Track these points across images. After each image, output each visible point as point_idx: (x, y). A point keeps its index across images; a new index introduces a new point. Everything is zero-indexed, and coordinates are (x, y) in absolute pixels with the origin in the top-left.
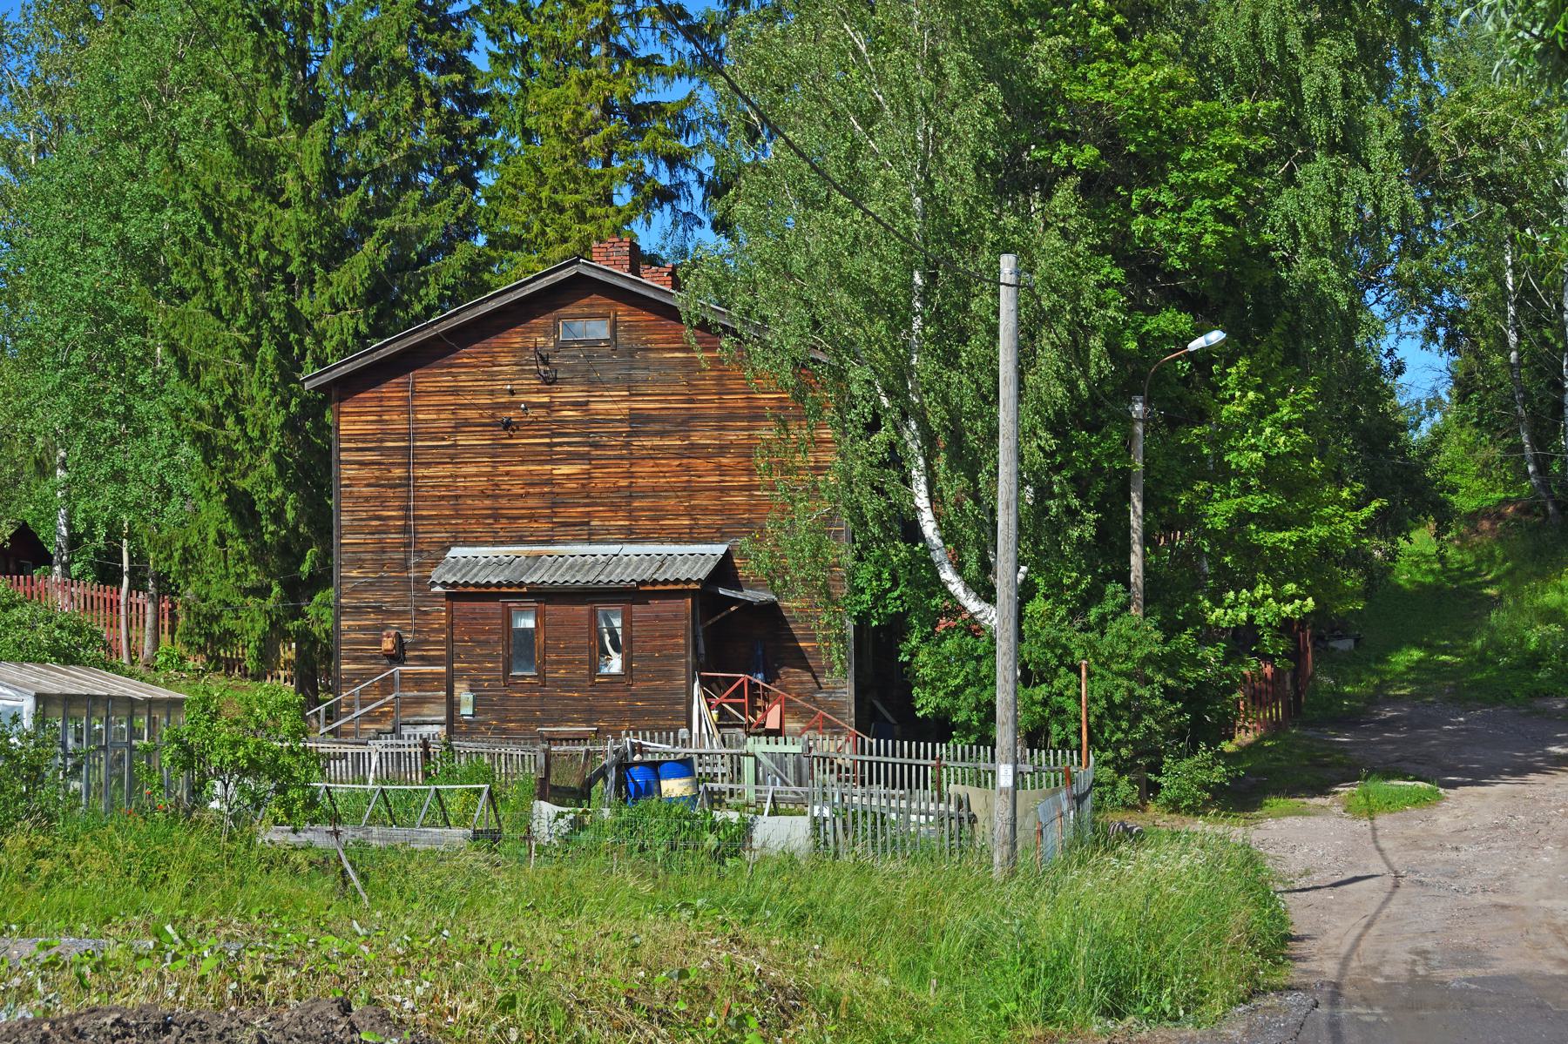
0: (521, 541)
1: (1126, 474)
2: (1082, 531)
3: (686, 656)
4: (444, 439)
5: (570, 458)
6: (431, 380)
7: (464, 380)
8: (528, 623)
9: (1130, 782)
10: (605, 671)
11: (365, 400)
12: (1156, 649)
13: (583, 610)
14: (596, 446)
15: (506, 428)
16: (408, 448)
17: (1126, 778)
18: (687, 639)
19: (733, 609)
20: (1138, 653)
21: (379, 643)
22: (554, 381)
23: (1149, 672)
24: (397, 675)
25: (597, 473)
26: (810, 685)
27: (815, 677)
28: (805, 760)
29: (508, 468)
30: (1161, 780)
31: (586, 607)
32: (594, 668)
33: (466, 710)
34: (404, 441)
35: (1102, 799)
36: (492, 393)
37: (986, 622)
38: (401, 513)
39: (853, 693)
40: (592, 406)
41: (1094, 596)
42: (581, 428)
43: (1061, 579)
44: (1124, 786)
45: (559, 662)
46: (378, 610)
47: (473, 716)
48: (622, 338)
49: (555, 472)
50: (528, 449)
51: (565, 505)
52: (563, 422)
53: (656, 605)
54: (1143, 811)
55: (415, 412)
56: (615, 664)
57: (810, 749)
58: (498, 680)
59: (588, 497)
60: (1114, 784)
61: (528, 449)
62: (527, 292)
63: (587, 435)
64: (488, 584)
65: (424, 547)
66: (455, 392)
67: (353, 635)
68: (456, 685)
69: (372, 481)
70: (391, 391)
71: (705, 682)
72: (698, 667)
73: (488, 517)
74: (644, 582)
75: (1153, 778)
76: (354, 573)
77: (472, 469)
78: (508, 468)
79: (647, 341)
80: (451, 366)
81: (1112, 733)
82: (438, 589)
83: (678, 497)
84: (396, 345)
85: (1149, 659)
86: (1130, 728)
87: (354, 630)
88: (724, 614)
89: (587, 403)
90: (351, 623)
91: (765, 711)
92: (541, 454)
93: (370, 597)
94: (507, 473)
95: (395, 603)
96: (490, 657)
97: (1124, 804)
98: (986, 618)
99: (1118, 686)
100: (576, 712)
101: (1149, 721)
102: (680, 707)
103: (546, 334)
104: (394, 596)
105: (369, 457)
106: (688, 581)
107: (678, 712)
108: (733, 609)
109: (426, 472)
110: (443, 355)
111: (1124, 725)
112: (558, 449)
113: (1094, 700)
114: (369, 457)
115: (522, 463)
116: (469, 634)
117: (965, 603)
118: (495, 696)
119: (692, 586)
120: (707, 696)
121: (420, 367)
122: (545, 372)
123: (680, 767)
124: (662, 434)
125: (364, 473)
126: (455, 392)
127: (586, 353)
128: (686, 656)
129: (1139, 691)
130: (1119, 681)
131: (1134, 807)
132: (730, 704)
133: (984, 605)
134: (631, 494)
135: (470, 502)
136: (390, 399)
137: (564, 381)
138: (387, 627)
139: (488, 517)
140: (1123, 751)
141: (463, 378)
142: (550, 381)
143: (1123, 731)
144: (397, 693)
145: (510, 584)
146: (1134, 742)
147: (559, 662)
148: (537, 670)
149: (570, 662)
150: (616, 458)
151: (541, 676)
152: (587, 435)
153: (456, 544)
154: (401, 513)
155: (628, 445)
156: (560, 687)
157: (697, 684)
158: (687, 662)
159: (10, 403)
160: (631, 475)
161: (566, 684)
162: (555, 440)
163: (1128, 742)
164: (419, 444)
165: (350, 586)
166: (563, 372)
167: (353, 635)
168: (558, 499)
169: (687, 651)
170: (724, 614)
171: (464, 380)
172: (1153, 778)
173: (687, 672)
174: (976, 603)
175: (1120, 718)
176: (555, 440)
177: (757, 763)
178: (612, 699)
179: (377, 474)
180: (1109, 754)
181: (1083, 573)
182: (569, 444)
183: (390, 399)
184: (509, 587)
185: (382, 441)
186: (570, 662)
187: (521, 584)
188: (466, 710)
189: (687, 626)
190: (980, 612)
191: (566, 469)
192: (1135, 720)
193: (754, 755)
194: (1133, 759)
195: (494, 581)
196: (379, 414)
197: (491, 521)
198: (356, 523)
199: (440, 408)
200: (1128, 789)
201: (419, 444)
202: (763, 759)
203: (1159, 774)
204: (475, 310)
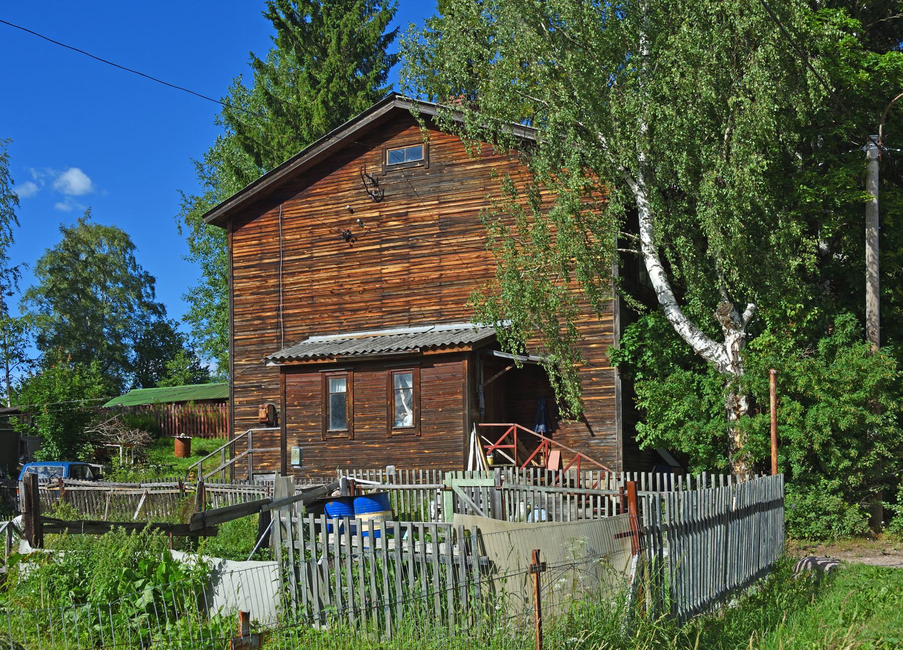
0: (358, 328)
1: (862, 207)
2: (804, 260)
3: (463, 410)
4: (304, 254)
5: (395, 259)
6: (294, 209)
7: (318, 206)
8: (343, 389)
9: (861, 510)
10: (400, 425)
11: (250, 229)
12: (889, 375)
13: (383, 375)
14: (413, 247)
15: (347, 241)
16: (278, 262)
17: (857, 505)
18: (464, 395)
19: (507, 369)
20: (870, 382)
21: (257, 414)
22: (383, 198)
23: (882, 400)
24: (250, 435)
25: (415, 269)
26: (585, 433)
27: (589, 426)
28: (498, 493)
29: (349, 272)
30: (894, 507)
31: (385, 372)
32: (391, 420)
33: (295, 461)
34: (276, 257)
35: (830, 527)
36: (337, 213)
37: (712, 359)
38: (274, 313)
39: (621, 438)
40: (411, 215)
41: (819, 330)
42: (402, 234)
43: (785, 312)
44: (853, 514)
45: (365, 420)
46: (259, 388)
47: (300, 465)
48: (433, 157)
49: (384, 271)
50: (364, 255)
51: (390, 297)
52: (390, 231)
53: (440, 368)
54: (875, 539)
55: (283, 235)
56: (408, 420)
57: (502, 481)
58: (319, 436)
59: (409, 289)
60: (841, 512)
61: (364, 255)
62: (358, 128)
63: (407, 239)
64: (306, 358)
65: (290, 337)
66: (311, 215)
67: (242, 409)
68: (288, 441)
69: (255, 290)
70: (266, 220)
71: (480, 431)
72: (473, 421)
73: (335, 311)
74: (425, 348)
75: (886, 505)
76: (243, 362)
77: (323, 275)
78: (349, 272)
79: (453, 159)
80: (309, 196)
81: (839, 461)
82: (271, 364)
83: (477, 283)
84: (265, 182)
85: (883, 386)
86: (860, 456)
87: (243, 405)
88: (500, 373)
89: (406, 214)
90: (241, 399)
91: (547, 457)
92: (374, 257)
93: (254, 380)
94: (349, 276)
95: (270, 383)
96: (313, 418)
97: (852, 532)
98: (712, 355)
99: (845, 413)
100: (378, 460)
101: (880, 447)
102: (460, 454)
103: (377, 163)
104: (270, 378)
105: (253, 272)
106: (461, 344)
107: (458, 457)
108: (507, 369)
109: (291, 280)
110: (303, 189)
111: (853, 453)
112: (386, 252)
113: (819, 429)
114: (253, 272)
115: (360, 266)
116: (298, 399)
117: (691, 342)
118: (317, 449)
119: (466, 349)
120: (483, 443)
121: (287, 199)
122: (376, 192)
123: (369, 501)
124: (463, 233)
125: (251, 284)
126: (311, 215)
127: (406, 173)
128: (463, 410)
129: (871, 418)
130: (847, 408)
131: (863, 535)
132: (501, 449)
133: (710, 343)
134: (440, 283)
135: (322, 301)
136: (266, 226)
137: (389, 198)
138: (264, 401)
139: (335, 311)
140: (852, 479)
141: (317, 204)
142: (379, 199)
143: (851, 459)
144: (250, 450)
145: (323, 357)
146: (865, 470)
147: (365, 420)
148: (348, 427)
149: (374, 418)
150: (429, 255)
151: (351, 431)
152: (407, 239)
153: (312, 334)
154: (274, 313)
155: (438, 244)
156: (365, 439)
157: (474, 431)
158: (464, 414)
159: (715, 377)
160: (440, 268)
161: (371, 438)
162: (384, 246)
163: (858, 470)
164: (286, 259)
165: (240, 371)
166: (389, 191)
167: (242, 409)
168: (386, 292)
169: (464, 406)
170: (500, 373)
171: (318, 206)
172: (886, 505)
173: (464, 422)
174: (702, 342)
175: (848, 446)
176: (384, 246)
177: (455, 495)
178: (405, 448)
179: (258, 284)
180: (836, 482)
181: (808, 306)
182: (394, 248)
183: (266, 226)
184: (323, 359)
185: (261, 259)
186: (374, 418)
187: (331, 356)
188: (295, 461)
189: (464, 383)
190: (707, 349)
191: (392, 268)
192: (866, 447)
193: (451, 490)
194: (862, 487)
195: (310, 354)
196: (259, 239)
197: (338, 314)
198: (244, 323)
199: (300, 228)
200: (858, 517)
201: (286, 259)
202: (461, 493)
203: (894, 501)
204: (320, 147)
